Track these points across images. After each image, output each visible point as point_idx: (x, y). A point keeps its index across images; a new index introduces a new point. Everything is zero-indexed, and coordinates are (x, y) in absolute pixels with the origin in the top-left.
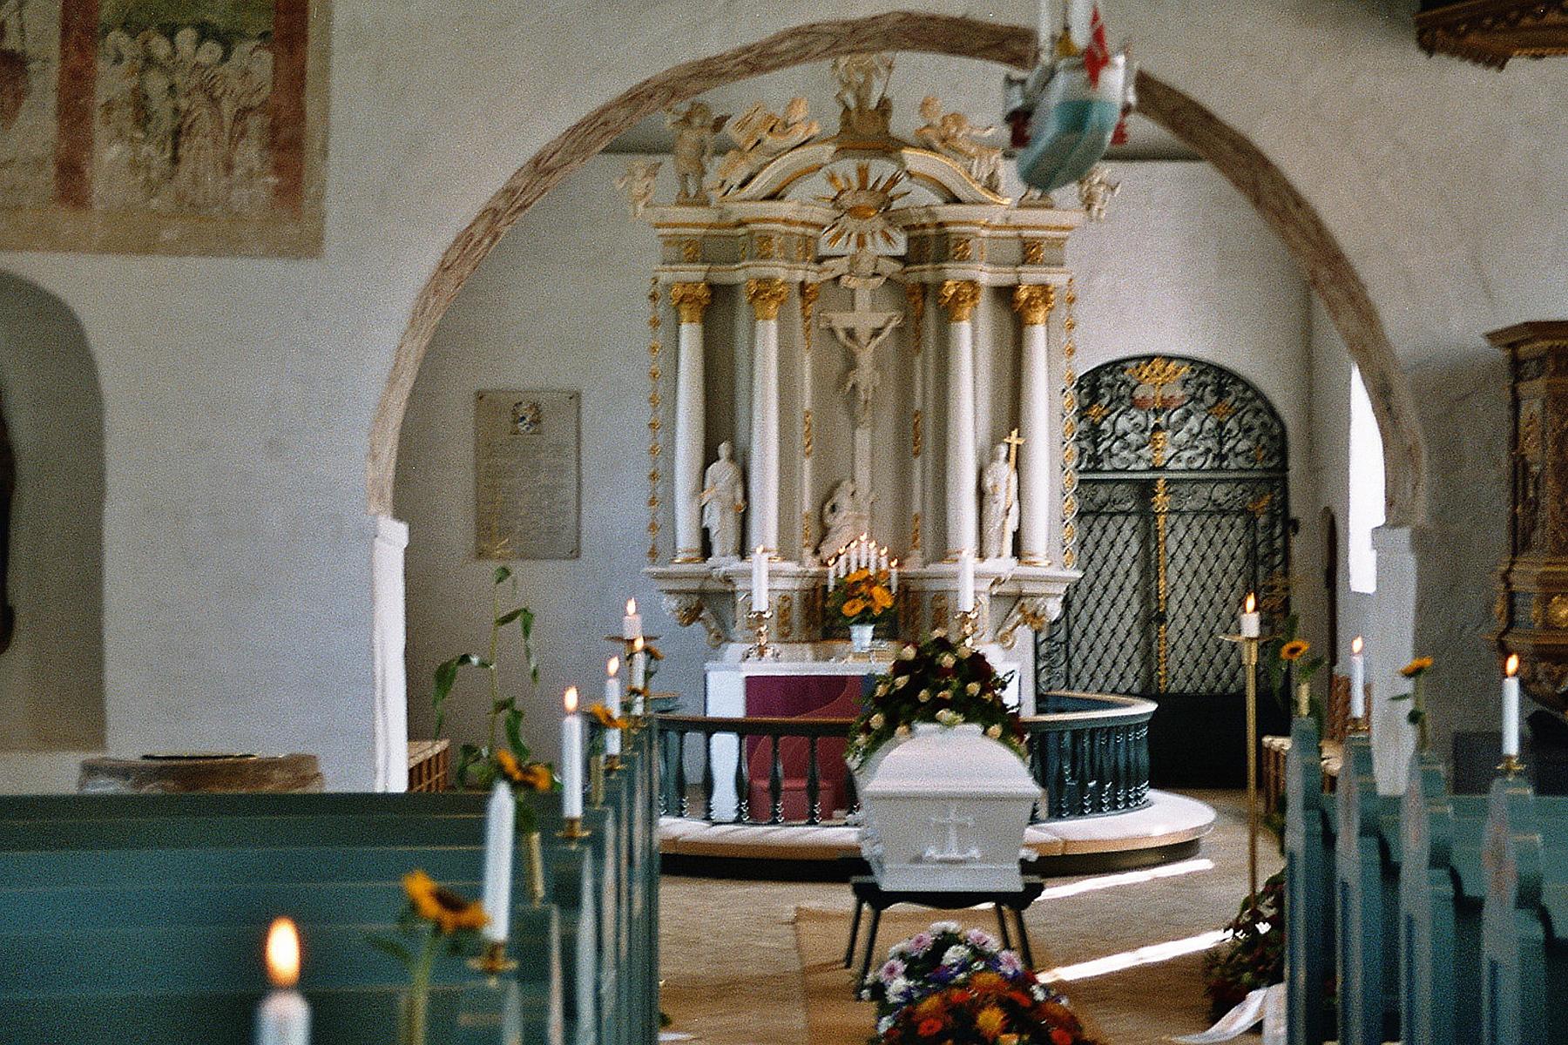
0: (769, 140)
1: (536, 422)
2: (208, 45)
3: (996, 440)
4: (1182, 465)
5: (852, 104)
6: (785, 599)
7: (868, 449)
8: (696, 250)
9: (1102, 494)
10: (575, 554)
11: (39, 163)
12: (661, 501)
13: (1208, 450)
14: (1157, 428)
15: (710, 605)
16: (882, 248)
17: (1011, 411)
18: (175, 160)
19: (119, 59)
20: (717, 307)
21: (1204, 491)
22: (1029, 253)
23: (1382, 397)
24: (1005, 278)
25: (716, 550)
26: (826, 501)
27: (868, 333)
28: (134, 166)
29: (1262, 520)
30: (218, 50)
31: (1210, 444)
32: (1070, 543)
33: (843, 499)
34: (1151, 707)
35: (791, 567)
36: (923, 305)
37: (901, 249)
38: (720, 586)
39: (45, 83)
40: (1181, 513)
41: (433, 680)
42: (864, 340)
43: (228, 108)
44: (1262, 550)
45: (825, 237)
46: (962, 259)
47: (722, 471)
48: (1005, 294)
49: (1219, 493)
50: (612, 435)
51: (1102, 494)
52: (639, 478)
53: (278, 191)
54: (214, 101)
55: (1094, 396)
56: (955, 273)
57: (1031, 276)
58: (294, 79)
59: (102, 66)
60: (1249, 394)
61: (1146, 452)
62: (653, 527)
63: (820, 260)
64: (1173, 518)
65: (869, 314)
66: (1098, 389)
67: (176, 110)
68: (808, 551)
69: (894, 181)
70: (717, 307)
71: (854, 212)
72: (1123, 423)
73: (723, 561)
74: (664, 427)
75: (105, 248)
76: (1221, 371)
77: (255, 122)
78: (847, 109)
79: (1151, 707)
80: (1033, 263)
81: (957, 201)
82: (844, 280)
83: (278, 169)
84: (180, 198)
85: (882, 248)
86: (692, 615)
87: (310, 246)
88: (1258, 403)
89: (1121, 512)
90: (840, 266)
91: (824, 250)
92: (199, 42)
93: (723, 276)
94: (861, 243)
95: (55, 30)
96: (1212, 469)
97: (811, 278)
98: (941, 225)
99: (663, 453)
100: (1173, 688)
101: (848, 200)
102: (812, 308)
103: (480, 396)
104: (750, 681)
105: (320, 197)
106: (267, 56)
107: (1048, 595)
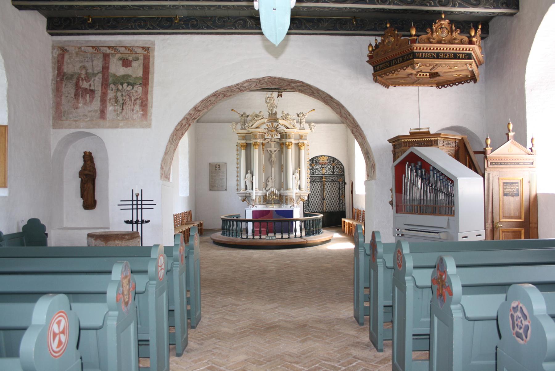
1: (219, 168)
2: (130, 86)
3: (295, 169)
7: (274, 170)
8: (244, 137)
9: (314, 178)
10: (226, 190)
11: (97, 111)
12: (238, 181)
15: (247, 198)
16: (276, 137)
17: (298, 165)
18: (123, 109)
19: (112, 90)
20: (248, 147)
22: (301, 137)
23: (367, 154)
24: (297, 141)
26: (267, 180)
28: (115, 111)
29: (341, 183)
30: (131, 87)
33: (270, 180)
34: (322, 215)
35: (261, 191)
36: (282, 145)
37: (279, 137)
39: (98, 95)
43: (133, 99)
45: (266, 135)
47: (249, 175)
48: (297, 144)
50: (231, 170)
51: (314, 178)
52: (234, 176)
53: (143, 115)
54: (130, 97)
55: (313, 162)
56: (288, 140)
57: (301, 141)
58: (146, 93)
59: (109, 91)
62: (237, 185)
63: (265, 139)
65: (274, 148)
67: (123, 99)
69: (278, 126)
70: (248, 147)
71: (271, 131)
72: (317, 167)
73: (249, 191)
74: (238, 168)
75: (109, 127)
76: (333, 158)
77: (138, 101)
79: (322, 215)
83: (143, 110)
84: (123, 117)
86: (244, 200)
87: (149, 126)
90: (269, 140)
91: (266, 137)
92: (128, 86)
93: (248, 142)
94: (272, 136)
95: (100, 85)
97: (264, 142)
99: (238, 172)
101: (270, 129)
102: (264, 147)
103: (210, 164)
104: (253, 211)
105: (151, 116)
106: (141, 88)
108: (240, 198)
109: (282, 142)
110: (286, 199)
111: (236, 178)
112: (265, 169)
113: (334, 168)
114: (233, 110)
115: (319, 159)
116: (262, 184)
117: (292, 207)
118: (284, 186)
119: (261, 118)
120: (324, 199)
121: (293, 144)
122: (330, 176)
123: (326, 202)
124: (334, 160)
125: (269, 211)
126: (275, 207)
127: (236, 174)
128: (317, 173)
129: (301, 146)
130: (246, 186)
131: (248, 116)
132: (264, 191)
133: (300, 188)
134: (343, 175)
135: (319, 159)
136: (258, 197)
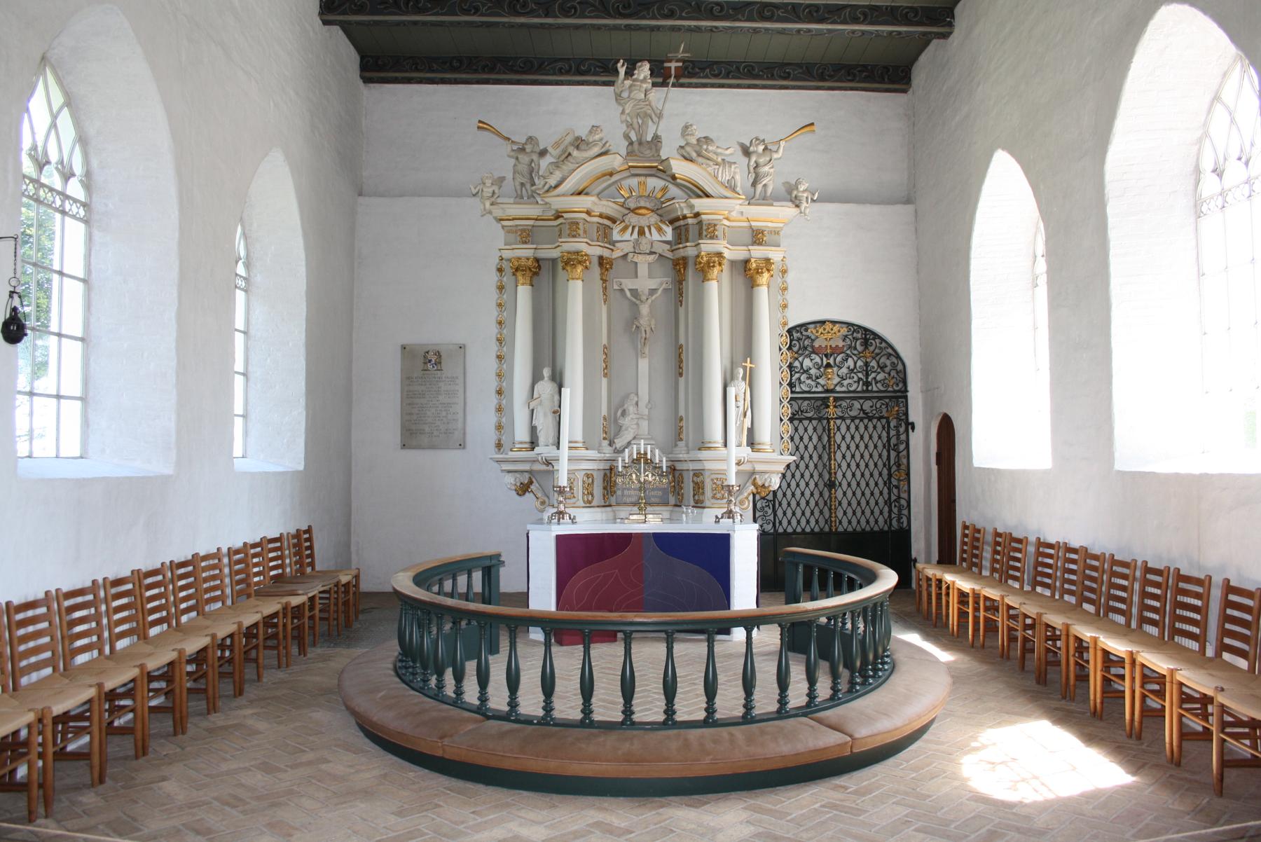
0: (575, 153)
1: (438, 363)
3: (733, 365)
4: (844, 389)
5: (634, 138)
6: (588, 476)
7: (646, 372)
8: (526, 236)
10: (462, 446)
13: (860, 379)
14: (828, 365)
15: (533, 482)
21: (857, 405)
22: (757, 237)
25: (542, 440)
27: (647, 292)
31: (860, 375)
32: (786, 437)
35: (592, 454)
36: (684, 270)
38: (544, 467)
40: (843, 418)
41: (569, 479)
42: (644, 298)
44: (893, 441)
46: (712, 238)
49: (867, 405)
52: (493, 392)
56: (707, 246)
57: (758, 252)
60: (884, 345)
61: (821, 381)
62: (499, 427)
64: (838, 422)
65: (648, 280)
66: (799, 338)
68: (606, 443)
72: (807, 363)
73: (543, 450)
76: (866, 330)
78: (631, 143)
80: (760, 244)
81: (708, 196)
82: (631, 255)
85: (656, 236)
86: (523, 489)
88: (890, 351)
89: (807, 418)
90: (627, 248)
93: (542, 254)
94: (641, 233)
96: (863, 391)
97: (606, 253)
98: (697, 215)
100: (840, 529)
103: (404, 348)
104: (560, 539)
107: (773, 472)
108: (510, 479)
109: (681, 253)
110: (699, 487)
111: (493, 400)
112: (605, 363)
113: (867, 369)
114: (483, 126)
115: (811, 331)
116: (600, 423)
117: (726, 522)
118: (689, 433)
119: (596, 150)
120: (831, 485)
121: (726, 267)
122: (854, 397)
123: (840, 494)
124: (865, 337)
125: (626, 538)
126: (654, 523)
127: (493, 384)
128: (806, 385)
129: (759, 272)
130: (533, 430)
131: (543, 153)
132: (608, 452)
133: (751, 443)
134: (900, 396)
135: (811, 331)
136: (580, 476)
